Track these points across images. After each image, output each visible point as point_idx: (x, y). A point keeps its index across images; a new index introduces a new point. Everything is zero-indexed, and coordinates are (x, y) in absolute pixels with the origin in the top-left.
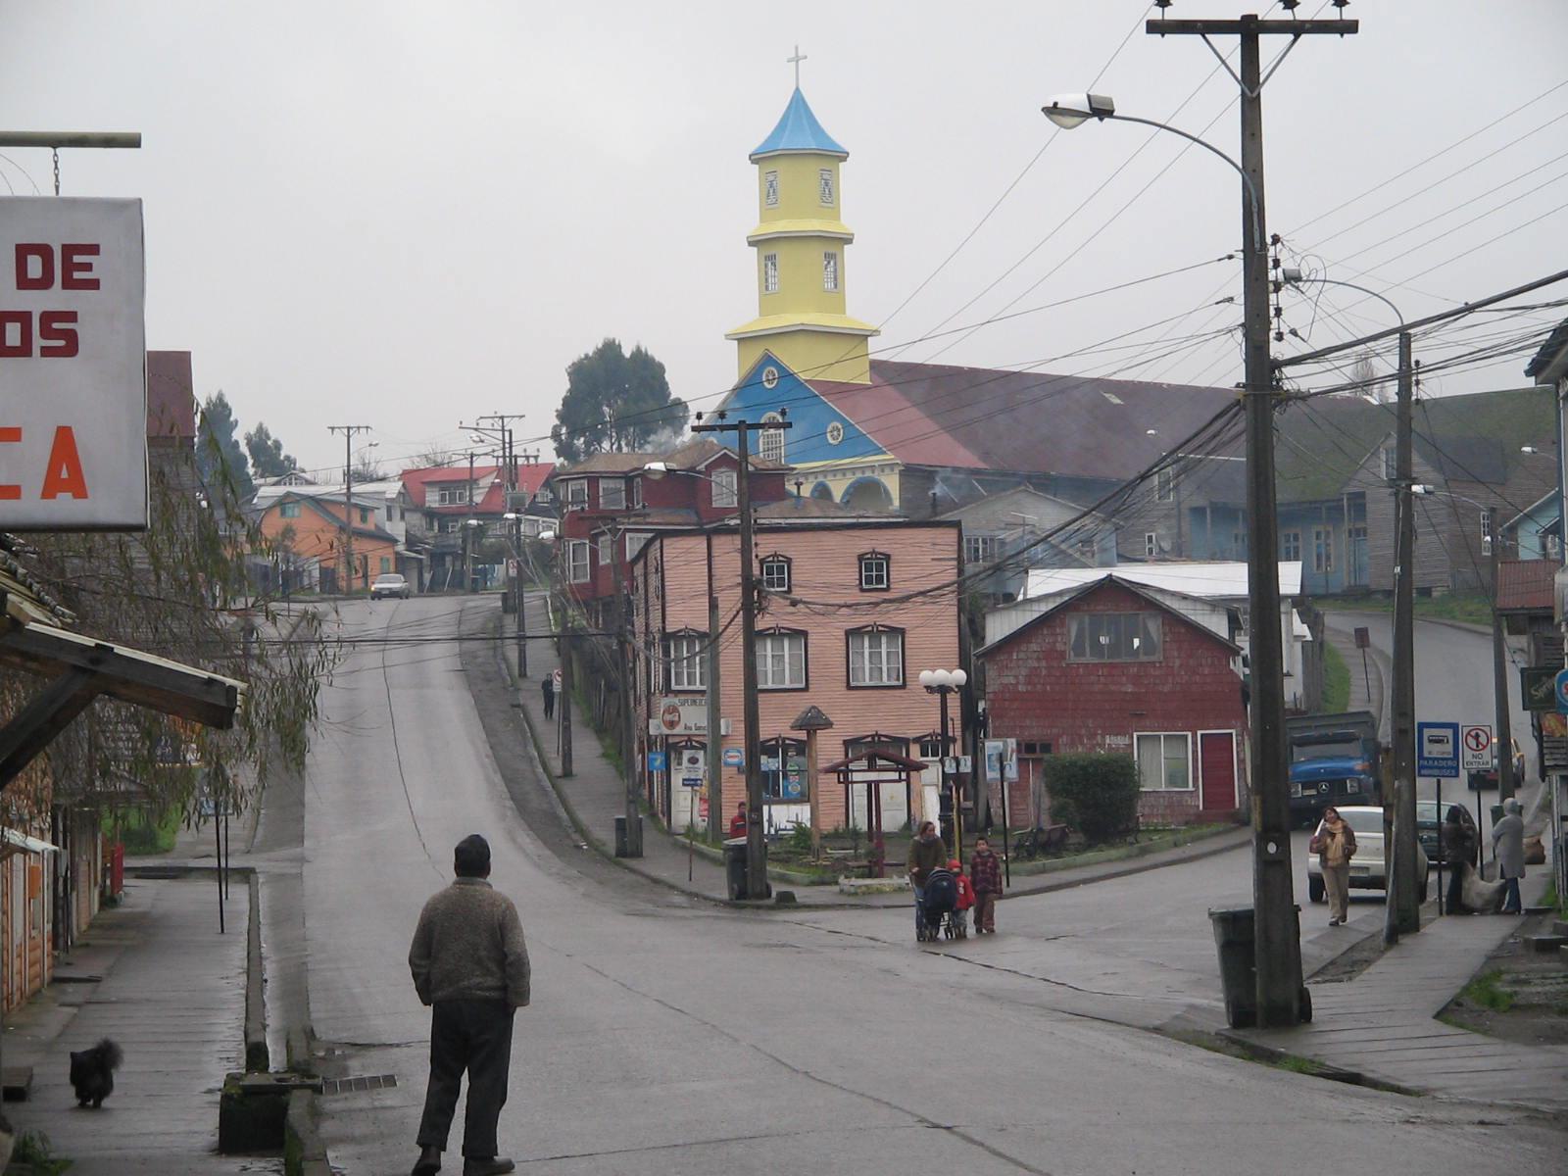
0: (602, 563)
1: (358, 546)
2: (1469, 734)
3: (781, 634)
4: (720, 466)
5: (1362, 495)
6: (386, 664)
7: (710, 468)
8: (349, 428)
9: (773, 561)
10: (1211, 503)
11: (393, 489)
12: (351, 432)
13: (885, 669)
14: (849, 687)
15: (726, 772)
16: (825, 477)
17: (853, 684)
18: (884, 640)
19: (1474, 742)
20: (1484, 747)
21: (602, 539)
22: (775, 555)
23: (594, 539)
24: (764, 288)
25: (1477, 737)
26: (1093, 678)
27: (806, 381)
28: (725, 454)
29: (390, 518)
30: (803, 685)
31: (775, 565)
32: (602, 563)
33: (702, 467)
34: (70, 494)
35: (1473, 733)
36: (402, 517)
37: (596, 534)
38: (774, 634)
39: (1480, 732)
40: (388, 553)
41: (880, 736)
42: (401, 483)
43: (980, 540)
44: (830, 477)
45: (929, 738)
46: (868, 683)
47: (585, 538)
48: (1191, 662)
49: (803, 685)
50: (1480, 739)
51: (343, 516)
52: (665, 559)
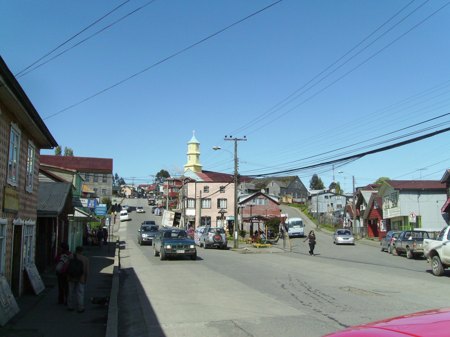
2: (411, 214)
3: (223, 199)
5: (268, 188)
6: (153, 179)
10: (248, 189)
13: (223, 206)
15: (282, 221)
19: (412, 216)
20: (414, 217)
22: (206, 186)
25: (413, 215)
26: (257, 208)
30: (210, 207)
34: (310, 250)
35: (412, 214)
38: (222, 199)
39: (413, 214)
43: (32, 235)
46: (207, 207)
48: (272, 206)
49: (210, 207)
50: (413, 215)
52: (110, 230)
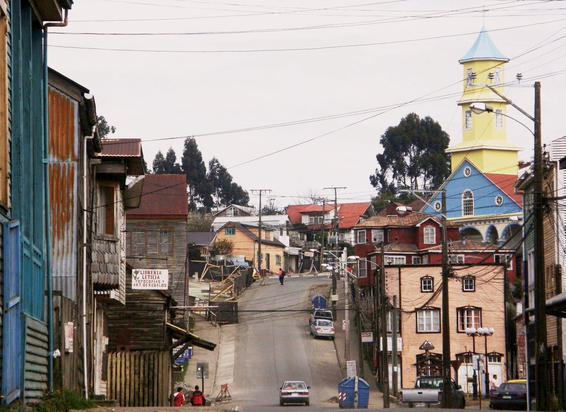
0: (372, 269)
1: (265, 250)
4: (428, 225)
7: (424, 225)
8: (261, 191)
9: (426, 279)
11: (283, 219)
12: (262, 192)
14: (417, 332)
16: (494, 222)
17: (419, 331)
18: (473, 312)
21: (372, 258)
22: (427, 276)
23: (369, 258)
24: (465, 127)
27: (485, 174)
28: (430, 219)
29: (281, 234)
31: (427, 280)
32: (372, 269)
33: (418, 225)
36: (288, 234)
37: (370, 255)
40: (280, 252)
41: (496, 353)
42: (287, 216)
44: (496, 222)
45: (492, 354)
47: (364, 257)
51: (257, 234)
